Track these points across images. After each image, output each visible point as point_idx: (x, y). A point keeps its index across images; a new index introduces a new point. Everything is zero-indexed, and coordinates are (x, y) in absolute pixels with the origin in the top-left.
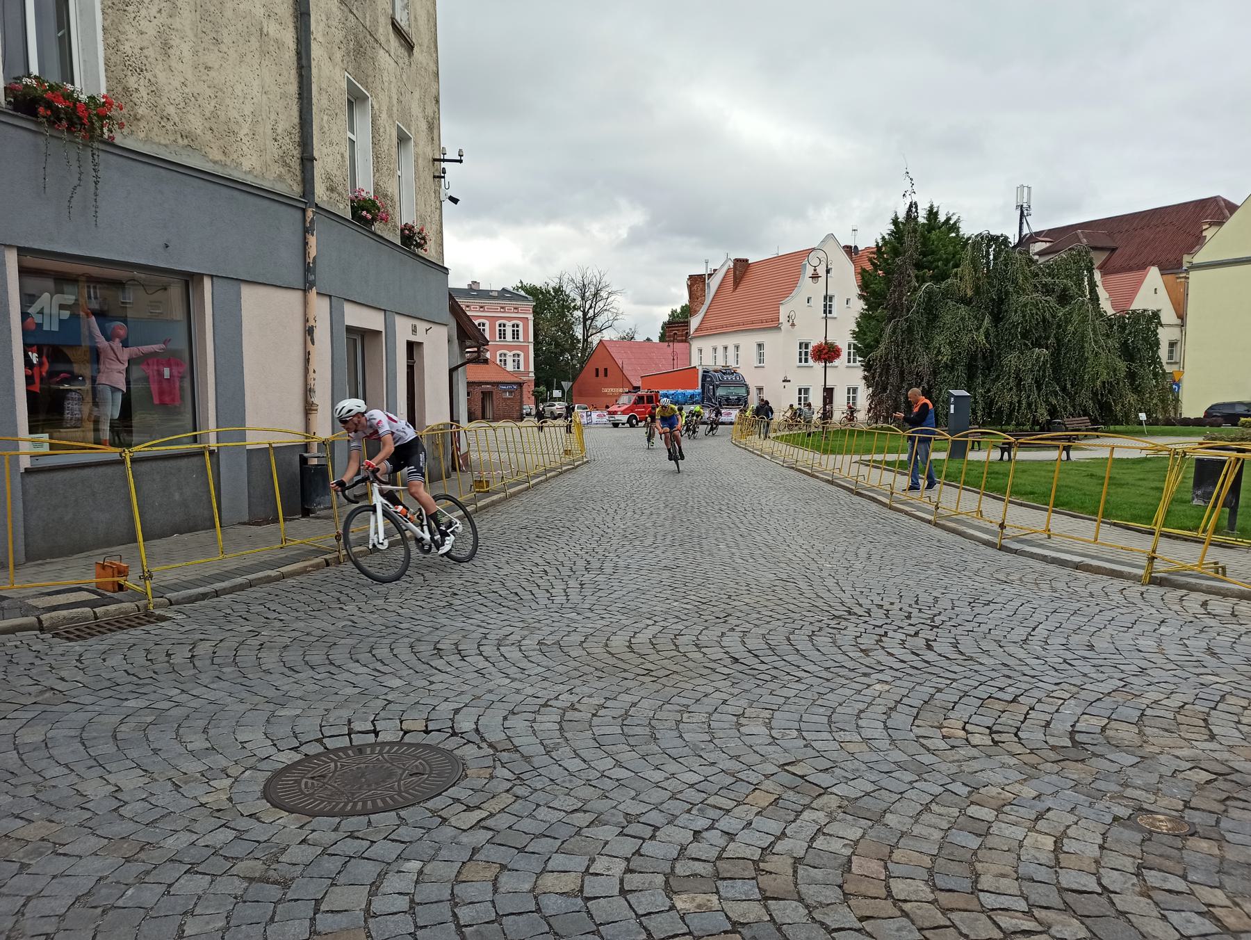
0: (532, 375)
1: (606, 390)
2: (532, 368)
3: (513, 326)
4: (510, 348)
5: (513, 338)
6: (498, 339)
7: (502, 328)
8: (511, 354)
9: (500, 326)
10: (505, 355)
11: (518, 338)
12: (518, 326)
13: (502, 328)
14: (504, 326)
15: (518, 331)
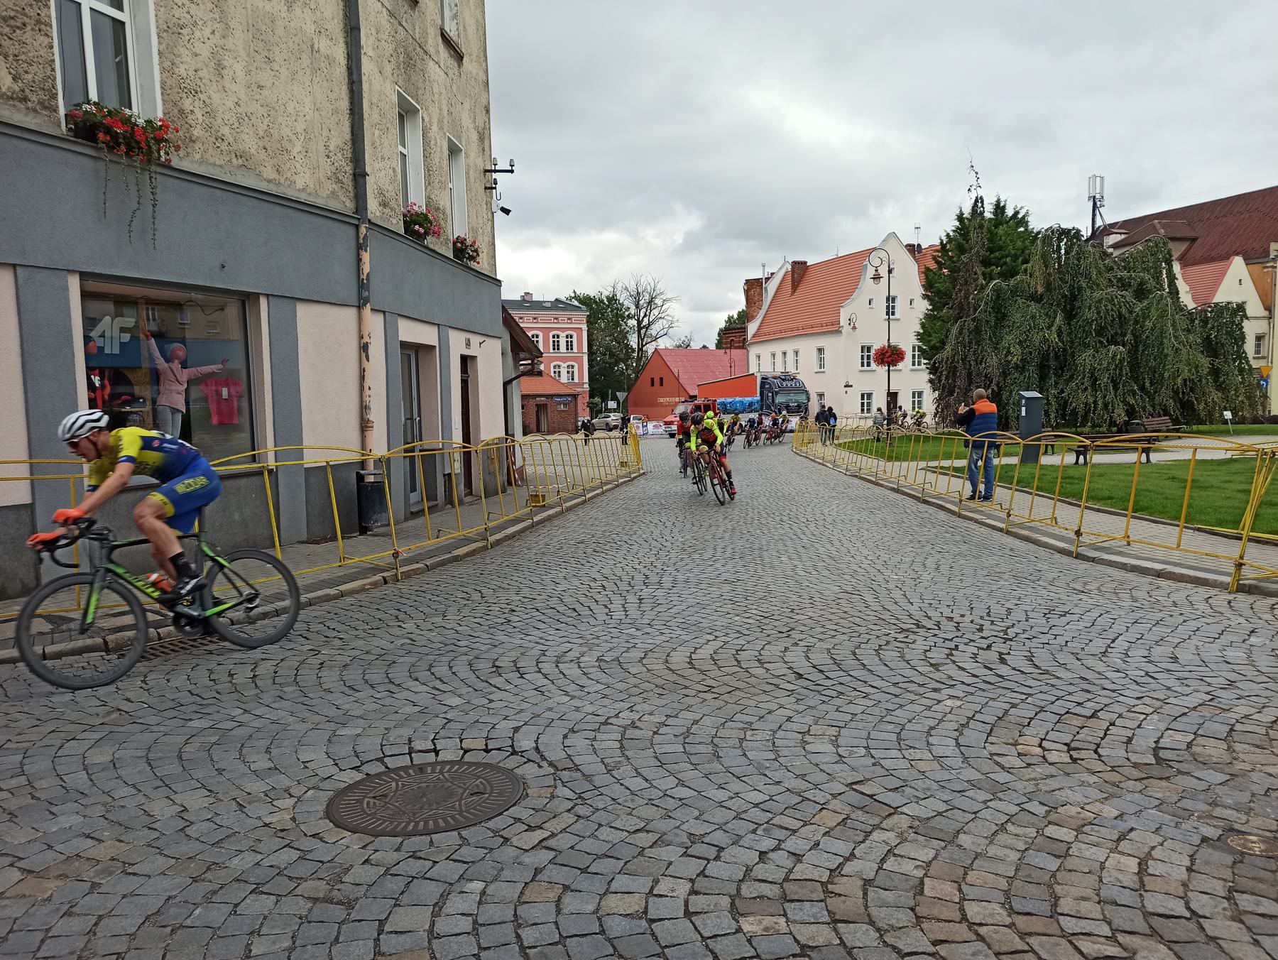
0: (587, 386)
1: (662, 400)
2: (586, 379)
3: (567, 337)
4: (564, 359)
5: (567, 349)
6: (551, 351)
7: (556, 339)
8: (566, 365)
9: (554, 337)
10: (559, 366)
11: (572, 349)
12: (571, 337)
13: (556, 339)
14: (558, 337)
15: (571, 342)
